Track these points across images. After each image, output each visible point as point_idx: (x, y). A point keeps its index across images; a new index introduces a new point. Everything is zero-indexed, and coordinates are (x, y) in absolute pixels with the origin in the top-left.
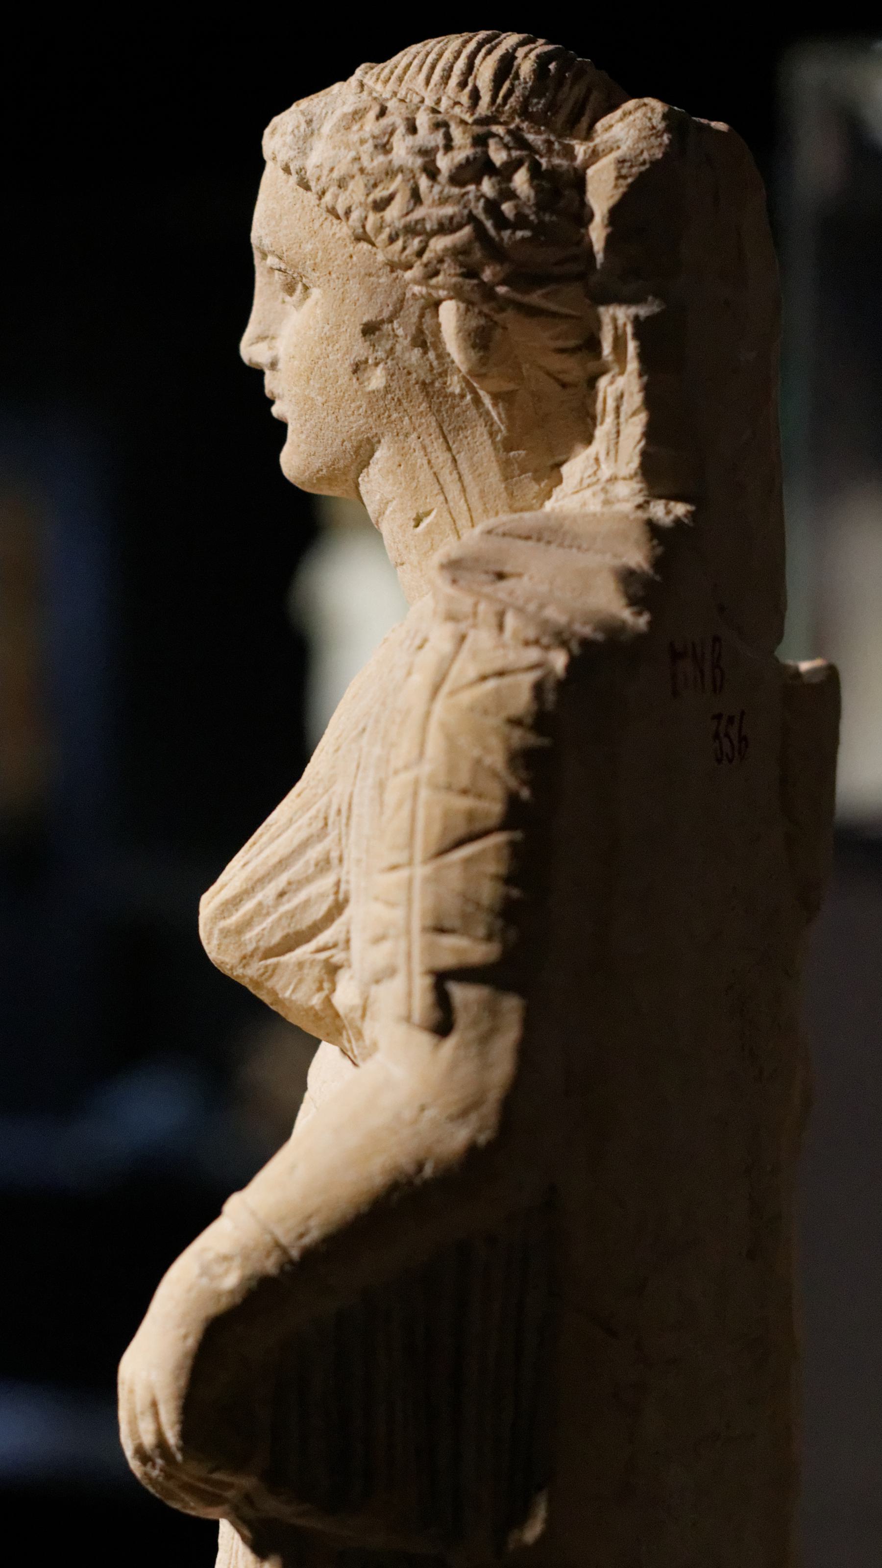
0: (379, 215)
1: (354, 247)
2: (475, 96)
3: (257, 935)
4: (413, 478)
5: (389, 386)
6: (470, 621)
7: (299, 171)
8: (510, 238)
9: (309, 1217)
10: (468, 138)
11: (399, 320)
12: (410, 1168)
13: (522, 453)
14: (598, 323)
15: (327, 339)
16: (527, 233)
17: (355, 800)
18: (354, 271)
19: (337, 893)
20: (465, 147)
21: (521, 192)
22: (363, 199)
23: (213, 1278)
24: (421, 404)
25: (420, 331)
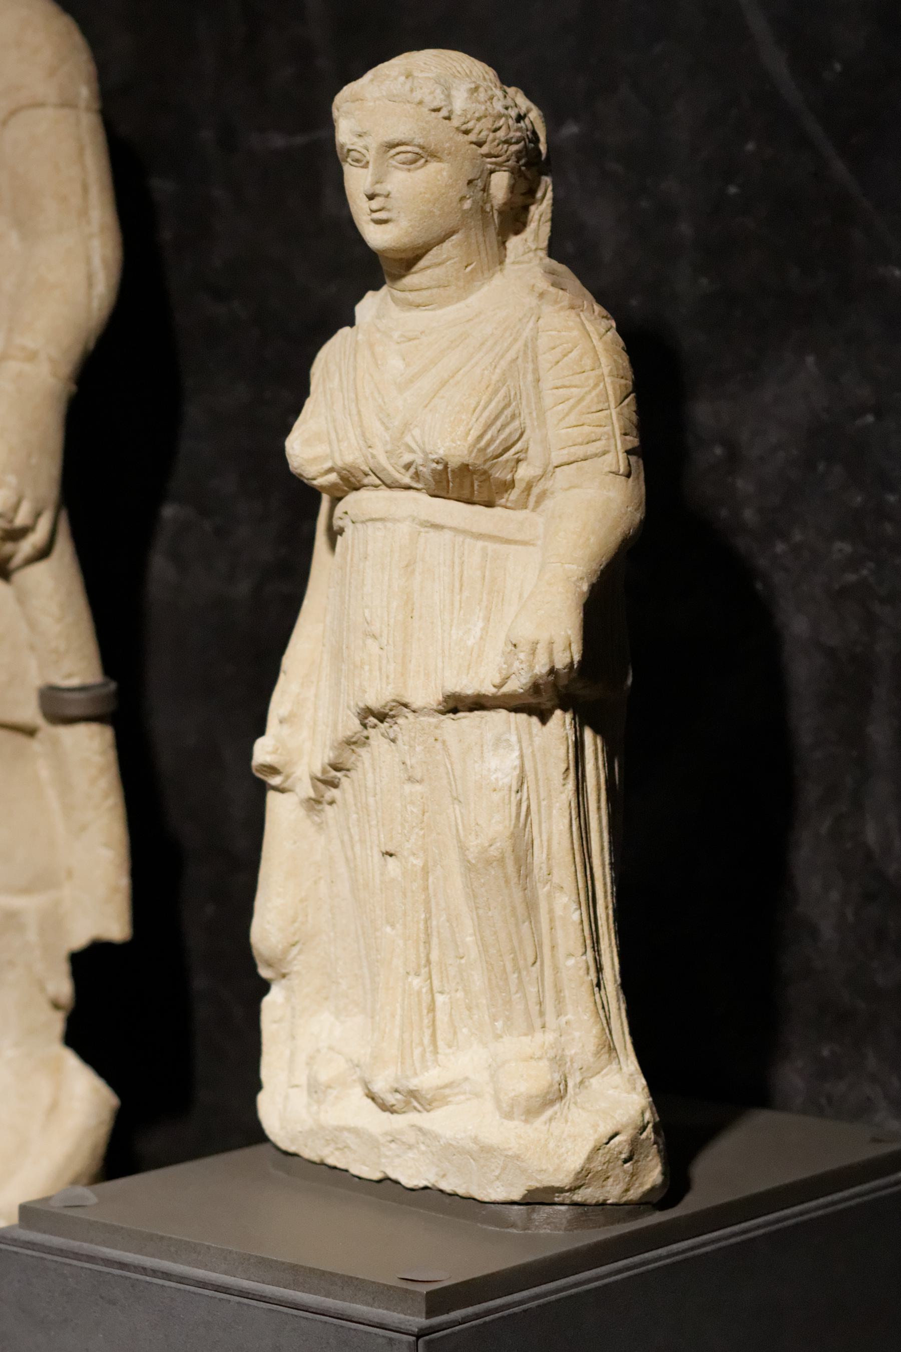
0: (494, 134)
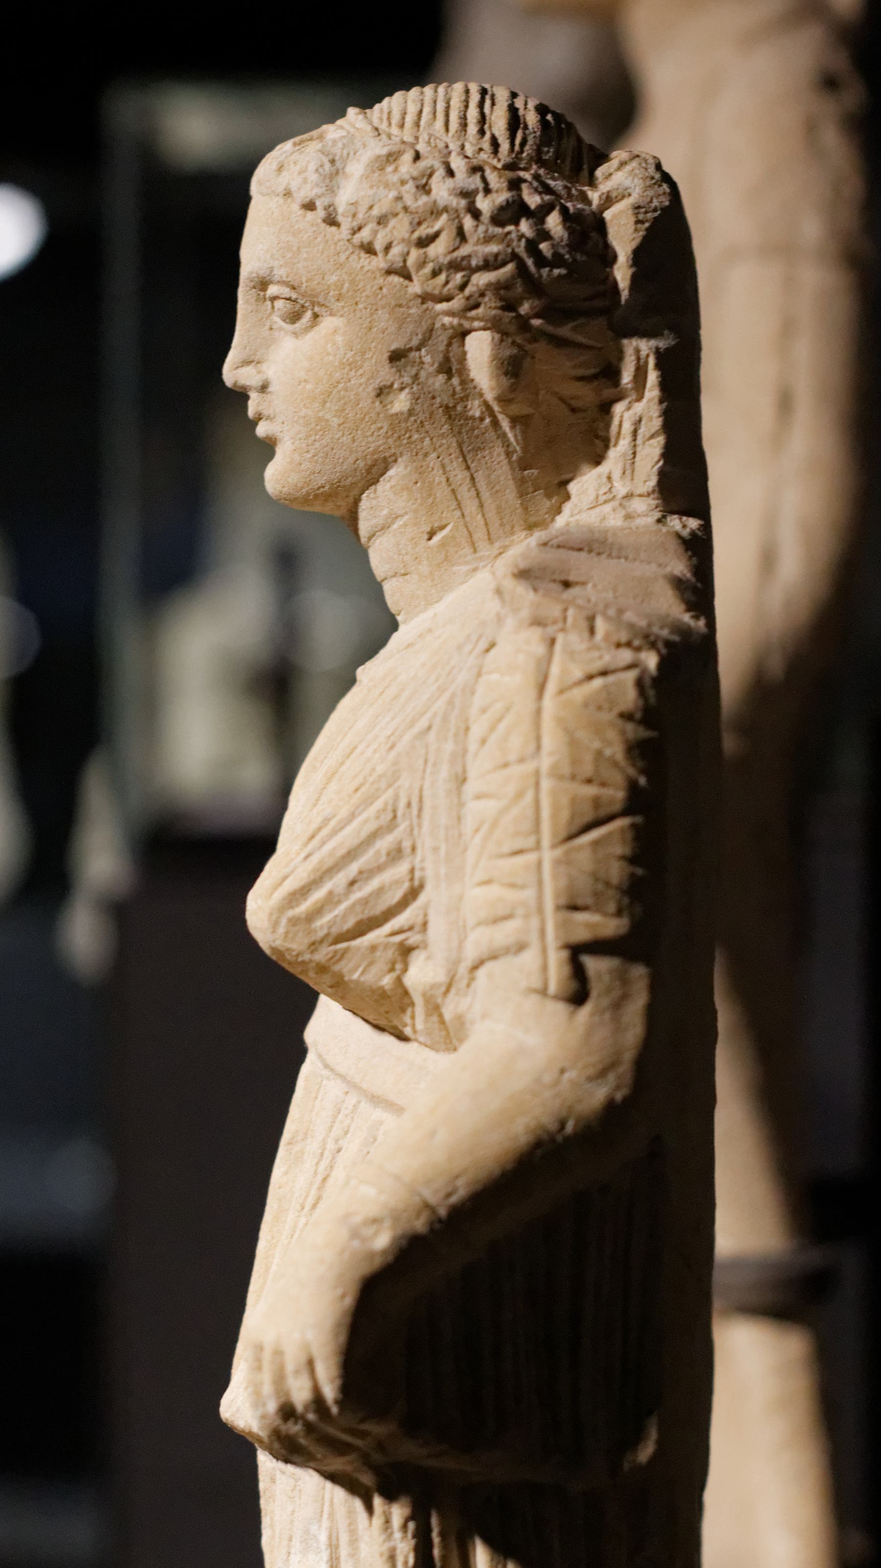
0: (422, 251)
1: (385, 280)
2: (495, 144)
3: (329, 922)
4: (430, 495)
5: (413, 409)
6: (560, 625)
7: (327, 207)
8: (548, 275)
9: (457, 1177)
10: (504, 182)
11: (427, 348)
12: (553, 1127)
13: (535, 472)
14: (620, 355)
15: (350, 364)
16: (563, 271)
17: (427, 793)
18: (383, 302)
19: (412, 879)
20: (502, 190)
21: (555, 233)
22: (407, 236)
23: (364, 1240)
24: (443, 426)
25: (447, 359)
